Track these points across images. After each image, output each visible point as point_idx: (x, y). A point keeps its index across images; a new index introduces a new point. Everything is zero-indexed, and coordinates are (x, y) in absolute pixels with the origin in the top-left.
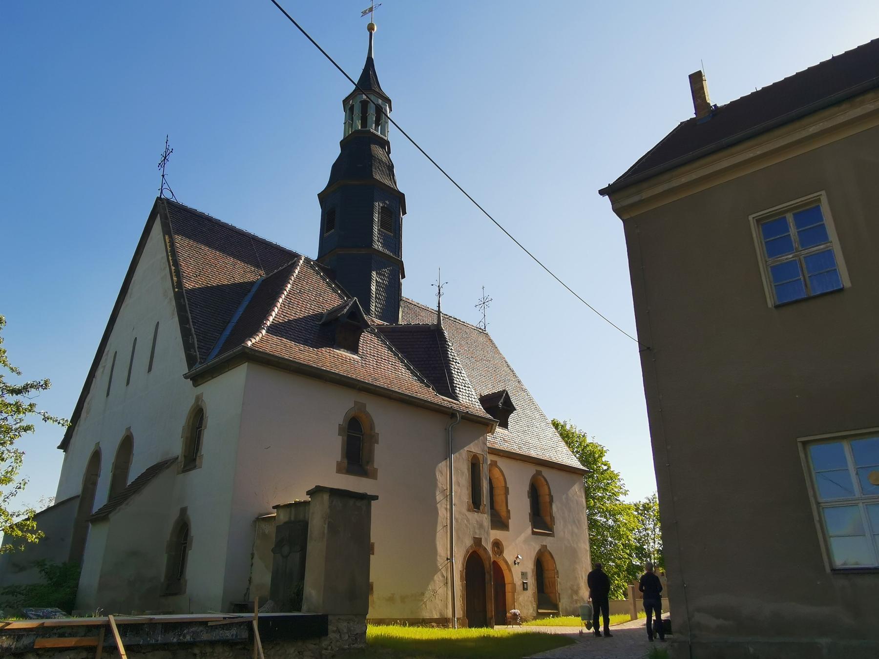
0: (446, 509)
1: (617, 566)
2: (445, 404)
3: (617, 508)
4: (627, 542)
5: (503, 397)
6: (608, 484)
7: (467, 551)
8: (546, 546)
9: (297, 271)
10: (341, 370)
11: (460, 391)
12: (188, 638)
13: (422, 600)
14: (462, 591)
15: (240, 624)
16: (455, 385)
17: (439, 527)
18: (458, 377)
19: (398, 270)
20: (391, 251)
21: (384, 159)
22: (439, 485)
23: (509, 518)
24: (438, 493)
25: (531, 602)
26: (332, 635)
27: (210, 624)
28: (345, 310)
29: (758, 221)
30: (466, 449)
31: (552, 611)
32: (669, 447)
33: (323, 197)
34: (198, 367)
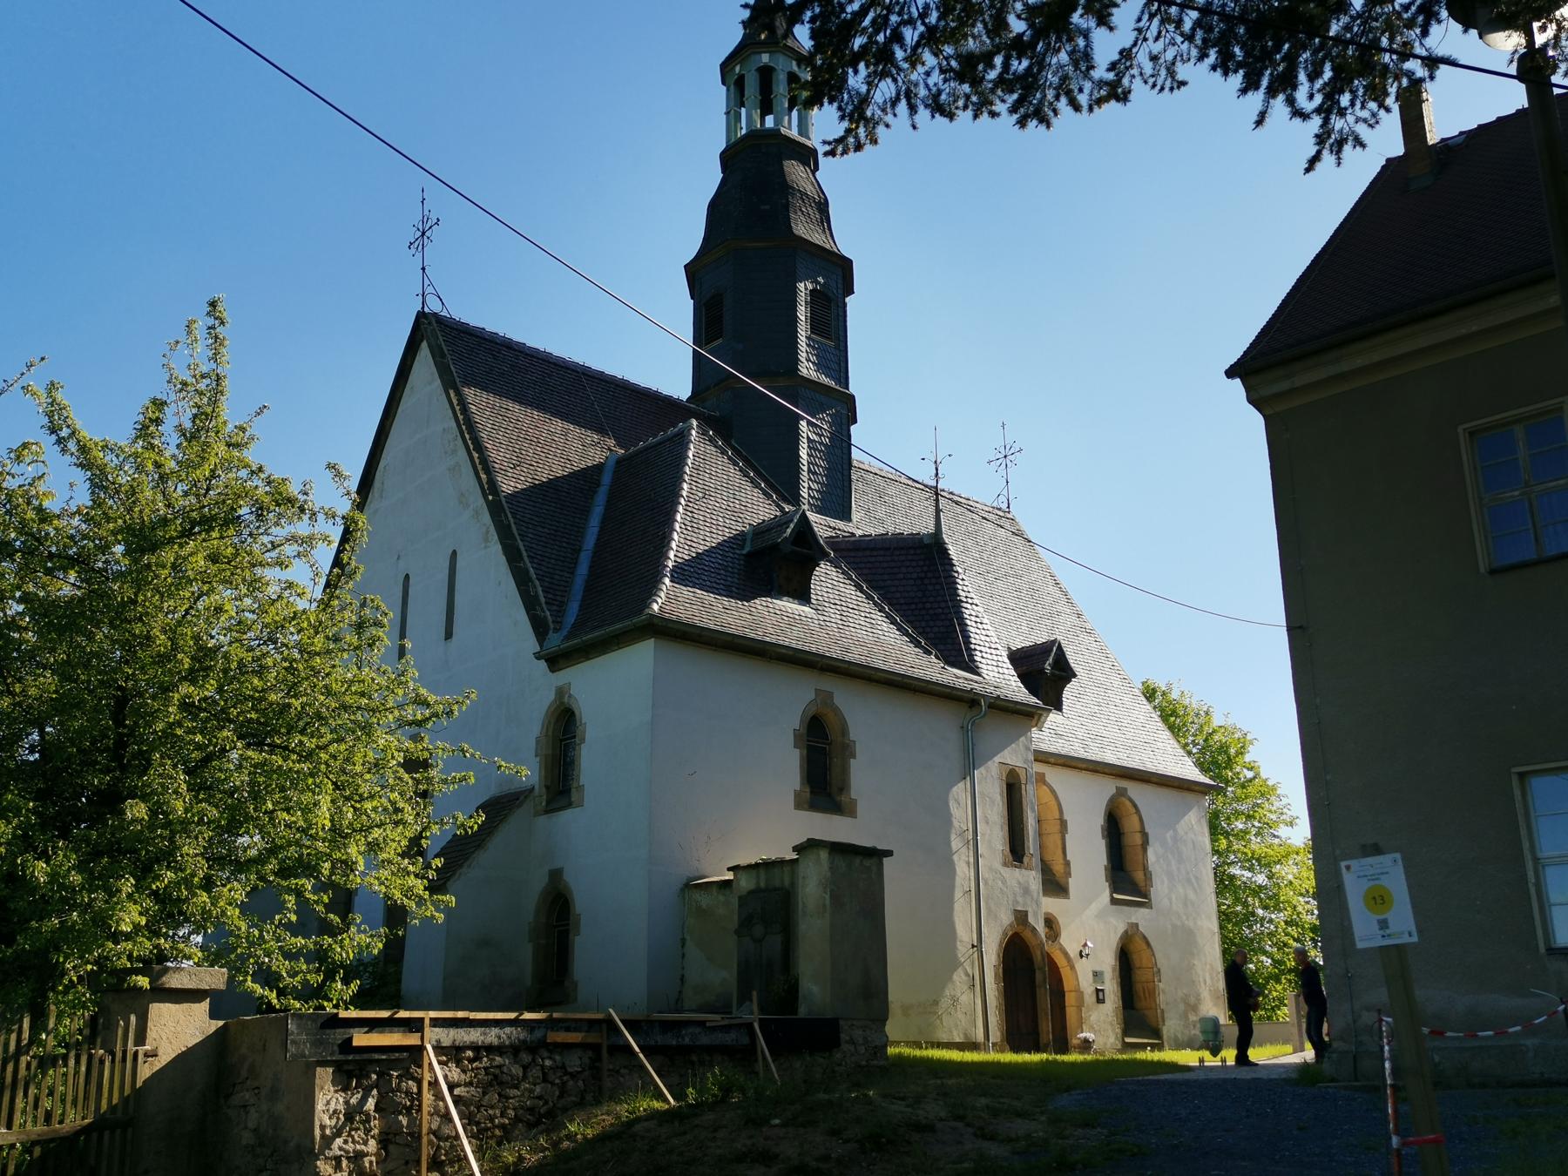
0: (968, 863)
1: (1276, 963)
2: (960, 684)
3: (1272, 853)
4: (1295, 917)
5: (1053, 654)
6: (1258, 805)
7: (1005, 934)
8: (1137, 925)
9: (690, 454)
10: (792, 638)
11: (982, 657)
12: (687, 1040)
13: (936, 1013)
14: (998, 999)
15: (741, 1025)
16: (973, 646)
17: (958, 894)
18: (978, 631)
19: (846, 410)
20: (832, 378)
21: (810, 190)
22: (956, 823)
23: (1068, 874)
24: (953, 837)
25: (1112, 1025)
26: (845, 1047)
27: (708, 1024)
28: (789, 531)
29: (1472, 434)
30: (997, 759)
31: (1150, 1041)
32: (1328, 777)
33: (694, 272)
34: (555, 641)
